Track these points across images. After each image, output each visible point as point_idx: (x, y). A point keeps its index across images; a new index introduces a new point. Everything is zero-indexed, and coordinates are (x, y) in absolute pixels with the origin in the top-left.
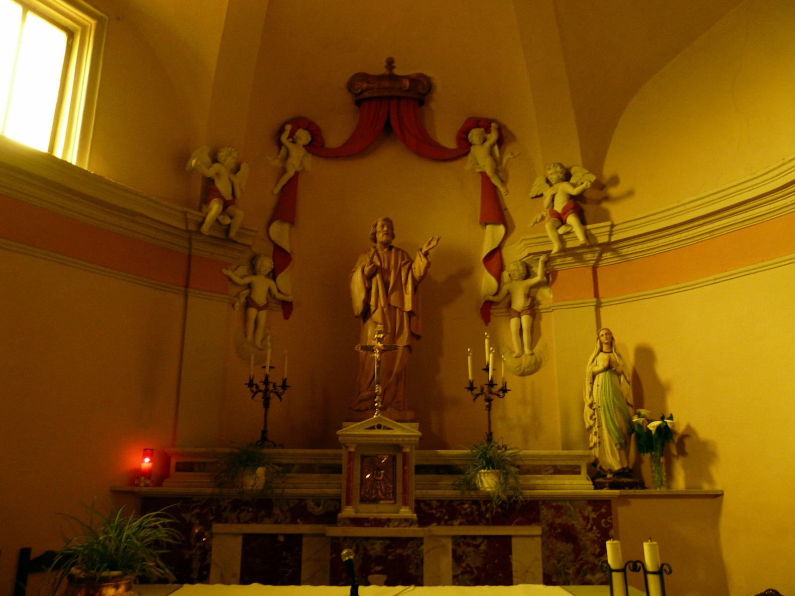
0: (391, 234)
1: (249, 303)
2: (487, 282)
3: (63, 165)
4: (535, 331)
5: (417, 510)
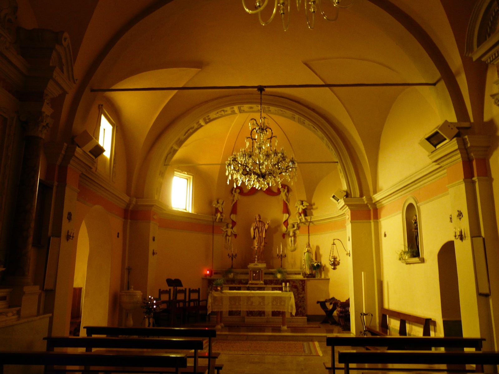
0: (260, 218)
1: (227, 235)
2: (284, 228)
3: (189, 213)
4: (295, 241)
5: (264, 282)
